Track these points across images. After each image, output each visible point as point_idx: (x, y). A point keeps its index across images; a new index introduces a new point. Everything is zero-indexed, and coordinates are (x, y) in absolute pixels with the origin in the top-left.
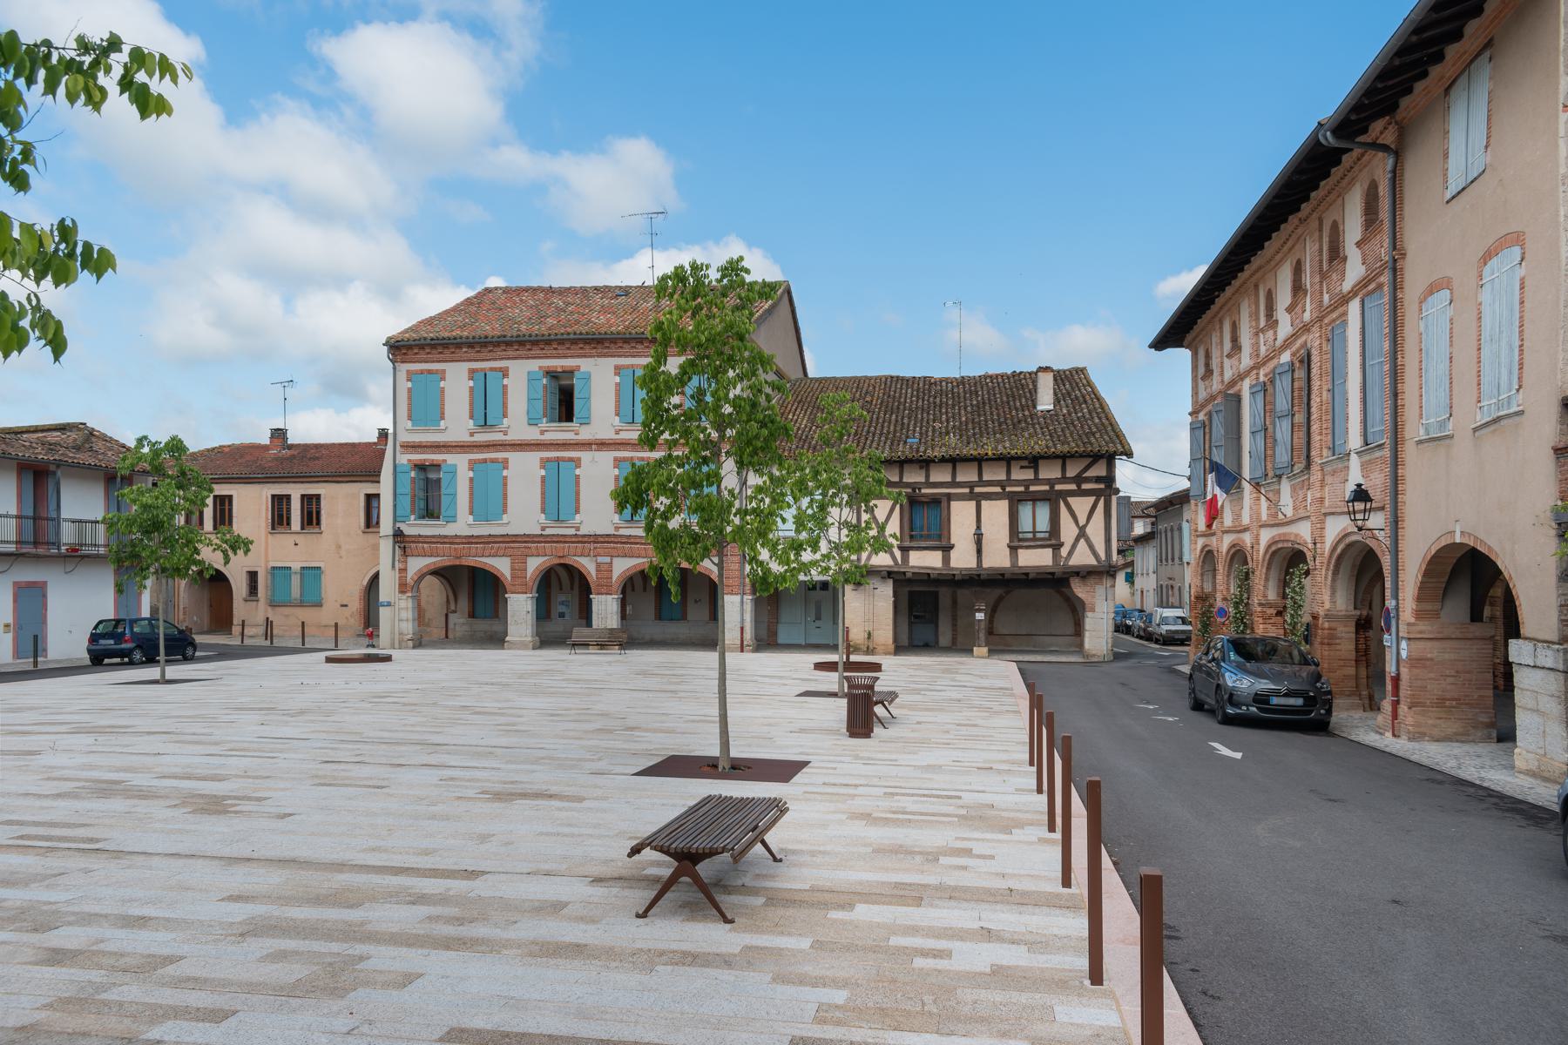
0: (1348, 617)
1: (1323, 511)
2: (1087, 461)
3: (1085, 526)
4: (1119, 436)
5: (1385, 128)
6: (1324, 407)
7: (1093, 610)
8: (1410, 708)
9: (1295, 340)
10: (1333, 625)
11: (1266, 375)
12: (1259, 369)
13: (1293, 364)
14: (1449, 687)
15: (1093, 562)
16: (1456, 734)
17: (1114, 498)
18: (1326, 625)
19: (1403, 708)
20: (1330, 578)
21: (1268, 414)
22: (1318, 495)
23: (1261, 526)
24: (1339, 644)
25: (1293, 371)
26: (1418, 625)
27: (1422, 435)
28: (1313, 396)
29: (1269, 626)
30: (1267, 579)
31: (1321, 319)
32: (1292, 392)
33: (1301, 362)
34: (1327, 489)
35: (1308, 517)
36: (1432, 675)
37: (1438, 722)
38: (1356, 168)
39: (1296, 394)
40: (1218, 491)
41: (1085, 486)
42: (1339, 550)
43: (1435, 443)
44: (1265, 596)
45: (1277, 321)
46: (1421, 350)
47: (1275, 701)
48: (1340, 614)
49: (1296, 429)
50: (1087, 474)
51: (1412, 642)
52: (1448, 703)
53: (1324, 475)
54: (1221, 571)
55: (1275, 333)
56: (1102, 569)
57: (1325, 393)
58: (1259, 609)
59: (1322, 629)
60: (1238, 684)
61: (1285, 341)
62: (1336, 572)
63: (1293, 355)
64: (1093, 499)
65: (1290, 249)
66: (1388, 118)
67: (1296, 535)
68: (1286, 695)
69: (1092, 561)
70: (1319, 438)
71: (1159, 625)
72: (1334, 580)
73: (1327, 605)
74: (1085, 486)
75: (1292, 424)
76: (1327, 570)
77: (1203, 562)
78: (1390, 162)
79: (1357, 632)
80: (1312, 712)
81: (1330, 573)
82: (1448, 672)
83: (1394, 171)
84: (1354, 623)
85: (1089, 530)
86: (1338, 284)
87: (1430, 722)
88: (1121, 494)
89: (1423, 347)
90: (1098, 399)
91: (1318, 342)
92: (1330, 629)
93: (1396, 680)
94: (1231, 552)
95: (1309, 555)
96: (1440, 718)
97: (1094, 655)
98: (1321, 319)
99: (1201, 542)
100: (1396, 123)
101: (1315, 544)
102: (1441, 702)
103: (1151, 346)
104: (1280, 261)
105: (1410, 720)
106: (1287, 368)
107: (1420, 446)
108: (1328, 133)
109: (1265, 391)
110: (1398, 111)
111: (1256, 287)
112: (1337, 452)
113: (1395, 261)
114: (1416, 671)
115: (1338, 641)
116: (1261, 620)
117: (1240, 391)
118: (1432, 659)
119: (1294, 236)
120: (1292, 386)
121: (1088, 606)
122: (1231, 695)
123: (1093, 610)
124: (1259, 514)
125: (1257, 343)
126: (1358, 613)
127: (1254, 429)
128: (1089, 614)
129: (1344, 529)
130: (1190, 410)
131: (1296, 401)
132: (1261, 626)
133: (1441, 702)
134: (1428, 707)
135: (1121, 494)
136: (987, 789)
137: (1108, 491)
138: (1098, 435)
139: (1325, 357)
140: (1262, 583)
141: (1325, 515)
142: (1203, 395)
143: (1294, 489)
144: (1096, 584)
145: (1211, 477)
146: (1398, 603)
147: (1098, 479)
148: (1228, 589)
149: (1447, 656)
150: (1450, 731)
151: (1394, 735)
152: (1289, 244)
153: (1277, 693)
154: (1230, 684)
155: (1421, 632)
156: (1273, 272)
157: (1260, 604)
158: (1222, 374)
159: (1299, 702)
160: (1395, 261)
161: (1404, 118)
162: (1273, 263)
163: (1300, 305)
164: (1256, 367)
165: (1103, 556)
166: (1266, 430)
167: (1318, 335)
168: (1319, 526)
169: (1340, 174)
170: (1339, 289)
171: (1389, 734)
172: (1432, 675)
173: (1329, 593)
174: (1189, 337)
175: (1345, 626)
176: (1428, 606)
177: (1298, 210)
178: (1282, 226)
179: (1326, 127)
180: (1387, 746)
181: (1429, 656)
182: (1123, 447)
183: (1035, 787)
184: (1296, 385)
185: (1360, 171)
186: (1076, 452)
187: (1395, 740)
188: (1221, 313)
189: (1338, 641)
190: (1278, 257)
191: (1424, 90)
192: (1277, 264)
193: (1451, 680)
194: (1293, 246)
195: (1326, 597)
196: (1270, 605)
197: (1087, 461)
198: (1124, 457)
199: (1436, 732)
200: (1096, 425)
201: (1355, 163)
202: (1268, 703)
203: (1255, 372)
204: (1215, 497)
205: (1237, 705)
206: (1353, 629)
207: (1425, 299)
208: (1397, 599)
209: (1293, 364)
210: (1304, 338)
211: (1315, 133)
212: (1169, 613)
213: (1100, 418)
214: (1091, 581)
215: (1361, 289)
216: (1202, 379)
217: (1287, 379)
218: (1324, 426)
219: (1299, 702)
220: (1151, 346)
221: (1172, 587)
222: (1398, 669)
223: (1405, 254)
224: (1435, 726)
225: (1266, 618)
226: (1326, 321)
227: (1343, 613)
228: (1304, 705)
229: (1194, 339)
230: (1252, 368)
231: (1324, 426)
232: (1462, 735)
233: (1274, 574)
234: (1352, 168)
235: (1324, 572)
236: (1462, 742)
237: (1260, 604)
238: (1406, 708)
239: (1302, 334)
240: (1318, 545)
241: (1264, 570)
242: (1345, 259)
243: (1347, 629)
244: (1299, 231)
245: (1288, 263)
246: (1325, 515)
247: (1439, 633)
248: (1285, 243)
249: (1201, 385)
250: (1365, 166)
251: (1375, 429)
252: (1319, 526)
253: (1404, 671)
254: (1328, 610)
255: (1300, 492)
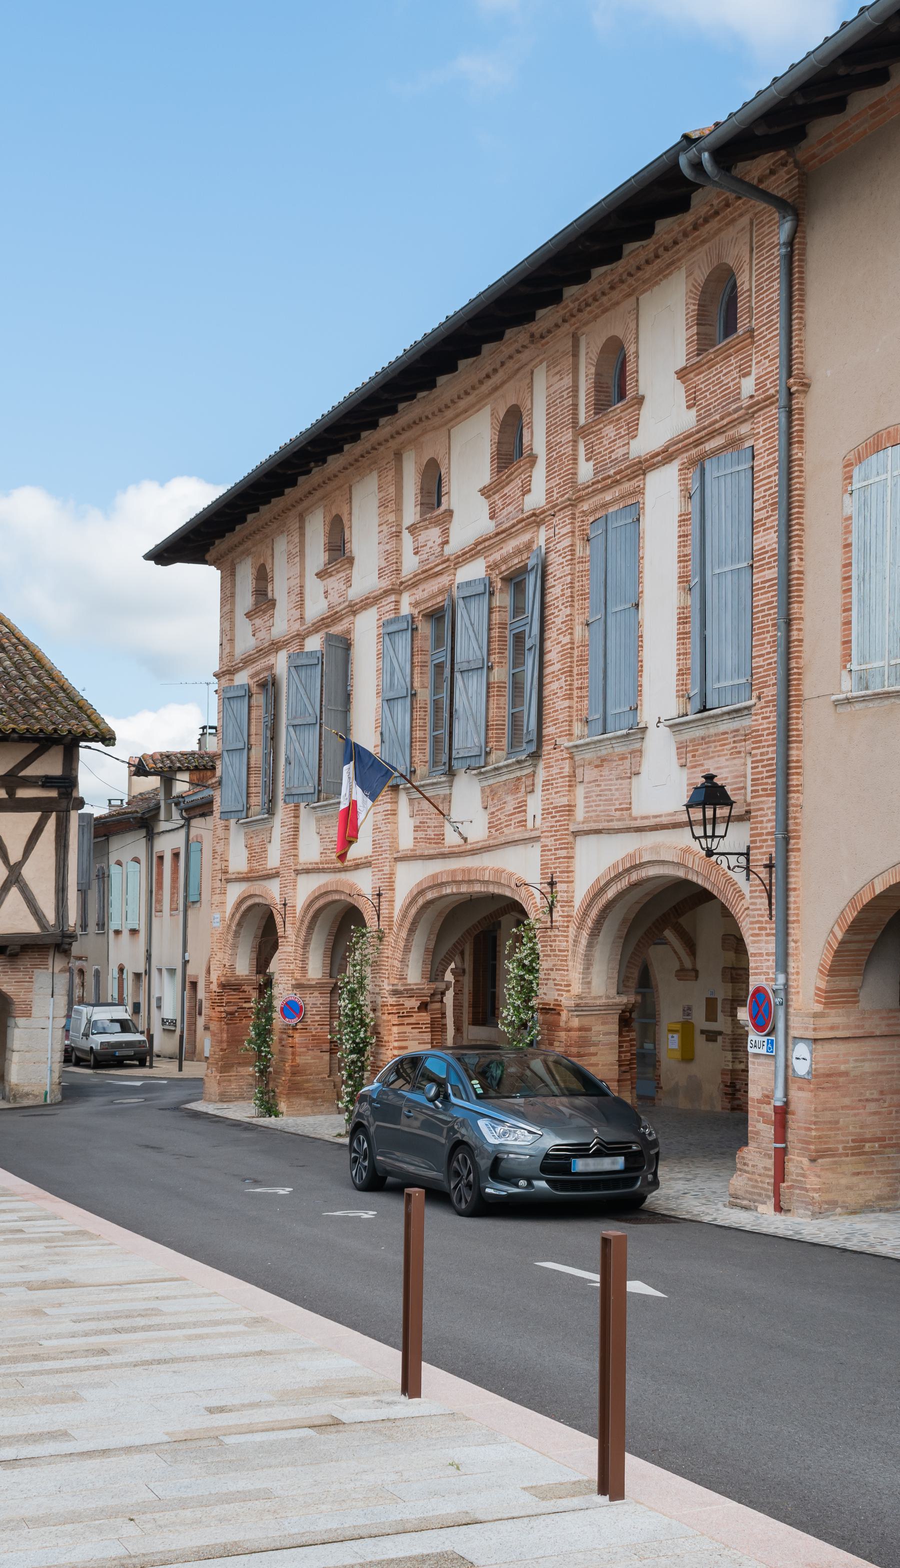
0: (608, 1006)
1: (573, 828)
2: (27, 749)
3: (20, 864)
4: (82, 708)
5: (772, 172)
6: (576, 652)
7: (28, 1014)
8: (813, 1160)
9: (503, 541)
10: (586, 1022)
11: (416, 605)
12: (400, 593)
13: (491, 583)
14: (869, 1120)
15: (34, 928)
16: (880, 1198)
17: (74, 816)
18: (575, 1023)
19: (797, 1162)
20: (584, 941)
21: (417, 670)
22: (564, 801)
23: (397, 860)
24: (595, 1054)
25: (492, 594)
26: (828, 1015)
27: (848, 686)
28: (552, 634)
29: (408, 1029)
30: (407, 949)
31: (573, 504)
32: (490, 629)
33: (506, 580)
34: (580, 791)
35: (536, 839)
36: (847, 1101)
37: (855, 1179)
38: (683, 245)
39: (495, 633)
40: (358, 794)
41: (23, 793)
42: (611, 893)
43: (887, 702)
44: (402, 978)
45: (450, 513)
46: (848, 546)
47: (580, 1165)
48: (598, 1002)
49: (494, 692)
50: (28, 772)
51: (819, 1046)
52: (868, 1147)
53: (574, 768)
54: (292, 938)
55: (446, 532)
56: (48, 941)
57: (578, 630)
58: (391, 1000)
59: (569, 1030)
60: (510, 1141)
61: (477, 544)
62: (595, 933)
63: (491, 567)
64: (35, 816)
65: (496, 389)
66: (783, 153)
67: (499, 872)
68: (598, 1154)
69: (31, 926)
70: (567, 703)
71: (86, 1035)
72: (590, 945)
73: (577, 988)
74: (23, 793)
75: (488, 684)
76: (580, 928)
77: (239, 925)
78: (787, 226)
79: (620, 1034)
80: (637, 1178)
81: (585, 934)
82: (868, 1095)
83: (790, 243)
84: (616, 1018)
85: (27, 872)
86: (619, 443)
87: (844, 1181)
88: (86, 810)
89: (854, 539)
90: (26, 647)
91: (567, 542)
92: (580, 1029)
93: (782, 1115)
94: (317, 906)
95: (369, 915)
96: (858, 1174)
97: (27, 1094)
98: (573, 504)
99: (235, 892)
100: (797, 164)
101: (552, 884)
102: (858, 1148)
103: (148, 557)
104: (466, 411)
105: (812, 1181)
106: (481, 589)
107: (840, 709)
108: (706, 156)
109: (414, 630)
110: (803, 144)
111: (398, 456)
112: (610, 726)
113: (790, 395)
114: (823, 1095)
115: (592, 1049)
116: (395, 1020)
117: (348, 632)
118: (846, 1074)
119: (511, 365)
120: (490, 620)
121: (17, 1008)
122: (497, 1161)
123: (28, 1014)
124: (394, 839)
125: (398, 551)
126: (624, 999)
127: (391, 695)
128: (21, 1021)
129: (632, 856)
130: (216, 668)
131: (495, 645)
132: (395, 1029)
133: (858, 1148)
134: (840, 1155)
135: (86, 810)
136: (478, 1505)
137: (64, 804)
138: (43, 705)
139: (579, 567)
140: (399, 955)
141: (576, 834)
142: (245, 643)
143: (490, 795)
144: (35, 966)
145: (348, 770)
146: (787, 980)
147: (47, 782)
148: (304, 969)
149: (868, 1067)
150: (871, 1194)
151: (779, 1208)
152: (496, 379)
153: (581, 1151)
154: (492, 1140)
155: (832, 1028)
156: (444, 430)
157: (395, 993)
158: (301, 604)
159: (618, 1163)
160: (790, 395)
161: (814, 156)
162: (449, 414)
163: (518, 482)
164: (396, 590)
165: (50, 916)
166: (414, 695)
167: (568, 529)
168: (563, 853)
169: (643, 256)
170: (621, 452)
171: (767, 1209)
172: (847, 1101)
173: (580, 968)
174: (221, 546)
175: (603, 1023)
176: (843, 983)
177: (531, 318)
178: (486, 348)
179: (702, 144)
180: (715, 1219)
181: (843, 1068)
182: (97, 726)
183: (592, 1473)
184: (496, 617)
185: (692, 249)
186: (14, 730)
187: (780, 1217)
188: (305, 504)
189: (592, 1049)
190: (462, 404)
191: (871, 107)
192: (458, 415)
193: (872, 1107)
194: (503, 383)
195: (575, 975)
196: (410, 993)
197: (28, 749)
198: (99, 745)
199: (851, 1199)
200: (33, 688)
201: (685, 234)
202: (567, 1170)
203: (393, 598)
204: (354, 804)
205: (510, 1179)
206: (615, 1028)
207: (860, 459)
208: (786, 972)
209: (491, 583)
210: (525, 538)
211: (674, 153)
212: (102, 1014)
213: (38, 677)
214: (26, 961)
215: (686, 448)
216: (248, 615)
217: (479, 609)
218: (576, 684)
219: (618, 1163)
220: (148, 557)
221: (81, 972)
222: (786, 1095)
223: (808, 386)
224: (849, 1188)
225: (403, 1015)
226: (585, 506)
227: (603, 1001)
228: (626, 1170)
229: (231, 549)
230: (386, 593)
231: (576, 684)
232: (889, 1198)
233: (420, 940)
234: (676, 243)
235: (572, 931)
236: (888, 1210)
237: (395, 993)
238: (805, 1161)
239: (524, 530)
240: (560, 887)
241: (404, 934)
242: (640, 400)
243: (606, 1028)
244: (525, 356)
245: (487, 410)
246: (576, 834)
247: (858, 1027)
248: (488, 376)
249: (243, 627)
250: (703, 242)
251: (723, 684)
252: (563, 853)
253: (801, 1101)
254: (579, 997)
255: (509, 798)
